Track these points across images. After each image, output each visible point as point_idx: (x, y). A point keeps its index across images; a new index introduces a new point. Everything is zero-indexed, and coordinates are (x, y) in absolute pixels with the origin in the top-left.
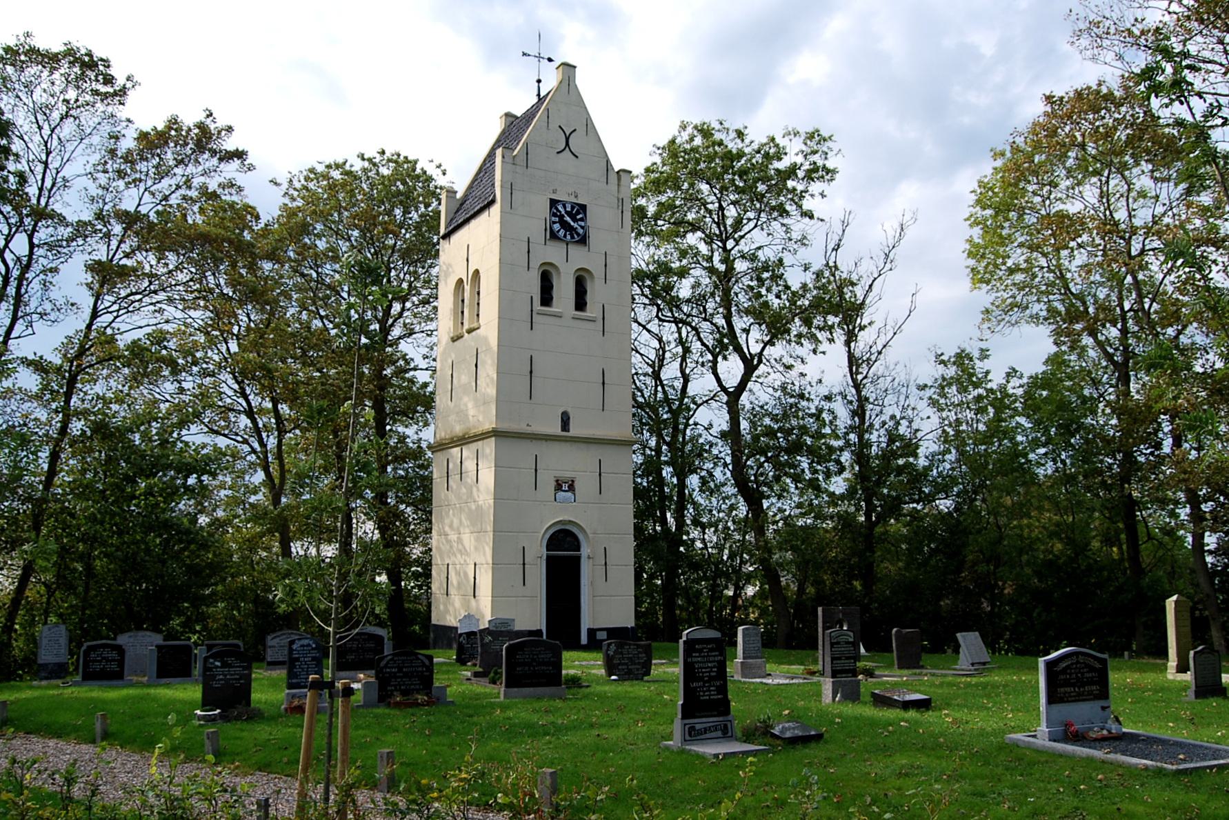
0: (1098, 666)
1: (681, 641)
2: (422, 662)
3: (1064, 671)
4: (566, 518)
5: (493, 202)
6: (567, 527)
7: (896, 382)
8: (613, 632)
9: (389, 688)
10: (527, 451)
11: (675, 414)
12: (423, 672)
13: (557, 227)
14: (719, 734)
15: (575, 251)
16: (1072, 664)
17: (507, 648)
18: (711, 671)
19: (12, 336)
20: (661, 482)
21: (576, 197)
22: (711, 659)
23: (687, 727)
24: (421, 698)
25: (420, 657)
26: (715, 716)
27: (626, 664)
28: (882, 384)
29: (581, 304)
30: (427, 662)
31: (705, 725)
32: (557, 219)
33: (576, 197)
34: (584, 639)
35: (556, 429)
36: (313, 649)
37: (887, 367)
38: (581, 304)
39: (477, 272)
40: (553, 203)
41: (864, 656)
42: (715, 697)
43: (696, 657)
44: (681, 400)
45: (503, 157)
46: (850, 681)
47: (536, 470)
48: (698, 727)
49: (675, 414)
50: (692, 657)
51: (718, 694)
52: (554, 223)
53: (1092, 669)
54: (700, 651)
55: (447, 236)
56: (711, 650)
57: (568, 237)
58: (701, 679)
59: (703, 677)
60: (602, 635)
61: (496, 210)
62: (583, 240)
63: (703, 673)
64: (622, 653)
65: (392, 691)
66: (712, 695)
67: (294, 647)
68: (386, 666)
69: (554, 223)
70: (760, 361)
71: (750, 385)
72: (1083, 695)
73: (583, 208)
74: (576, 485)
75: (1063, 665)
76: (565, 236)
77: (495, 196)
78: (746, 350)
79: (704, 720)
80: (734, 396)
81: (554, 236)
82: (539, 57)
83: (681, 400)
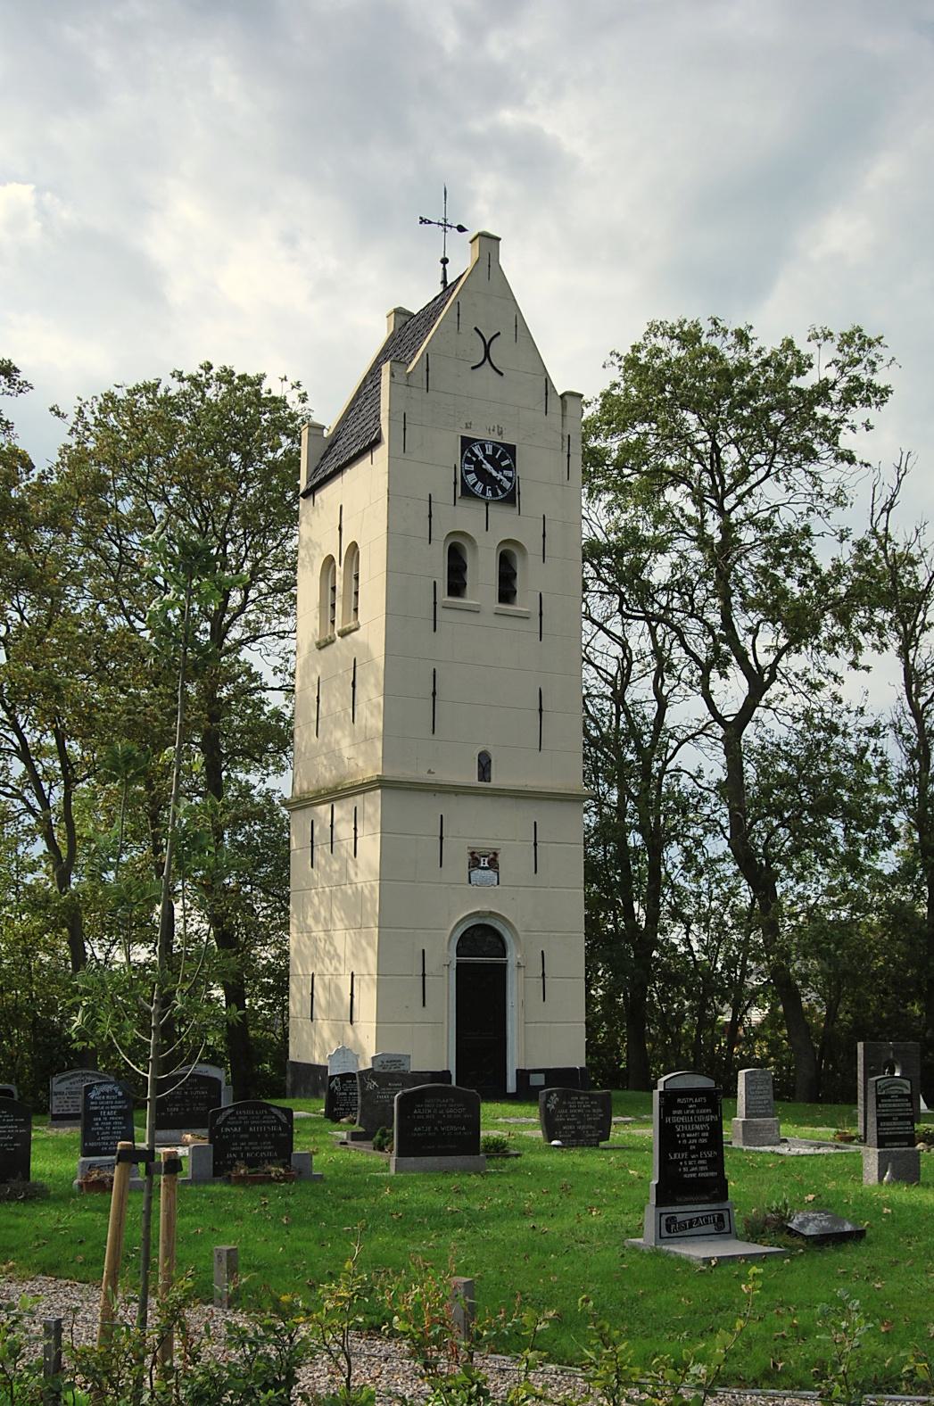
1: (656, 1093)
4: (486, 908)
5: (377, 442)
6: (487, 922)
8: (554, 1076)
10: (425, 811)
12: (277, 1132)
13: (471, 478)
14: (711, 1228)
15: (499, 513)
17: (400, 1099)
18: (100, 1122)
21: (500, 433)
22: (700, 1119)
23: (665, 1217)
24: (276, 1170)
25: (273, 1110)
27: (574, 1123)
29: (507, 593)
30: (284, 1119)
33: (500, 433)
34: (511, 1086)
35: (471, 778)
38: (507, 593)
39: (354, 546)
40: (467, 443)
42: (707, 1175)
43: (677, 1117)
45: (392, 375)
47: (441, 838)
48: (680, 1218)
49: (645, 755)
50: (672, 1115)
51: (709, 1171)
52: (468, 472)
54: (684, 1107)
55: (310, 492)
56: (700, 1106)
57: (489, 494)
58: (685, 1148)
60: (538, 1080)
61: (382, 453)
62: (511, 498)
63: (688, 1139)
64: (567, 1107)
65: (234, 1159)
66: (695, 1170)
67: (92, 1095)
68: (224, 1124)
73: (510, 450)
74: (499, 859)
76: (484, 492)
77: (380, 432)
81: (467, 492)
82: (445, 225)
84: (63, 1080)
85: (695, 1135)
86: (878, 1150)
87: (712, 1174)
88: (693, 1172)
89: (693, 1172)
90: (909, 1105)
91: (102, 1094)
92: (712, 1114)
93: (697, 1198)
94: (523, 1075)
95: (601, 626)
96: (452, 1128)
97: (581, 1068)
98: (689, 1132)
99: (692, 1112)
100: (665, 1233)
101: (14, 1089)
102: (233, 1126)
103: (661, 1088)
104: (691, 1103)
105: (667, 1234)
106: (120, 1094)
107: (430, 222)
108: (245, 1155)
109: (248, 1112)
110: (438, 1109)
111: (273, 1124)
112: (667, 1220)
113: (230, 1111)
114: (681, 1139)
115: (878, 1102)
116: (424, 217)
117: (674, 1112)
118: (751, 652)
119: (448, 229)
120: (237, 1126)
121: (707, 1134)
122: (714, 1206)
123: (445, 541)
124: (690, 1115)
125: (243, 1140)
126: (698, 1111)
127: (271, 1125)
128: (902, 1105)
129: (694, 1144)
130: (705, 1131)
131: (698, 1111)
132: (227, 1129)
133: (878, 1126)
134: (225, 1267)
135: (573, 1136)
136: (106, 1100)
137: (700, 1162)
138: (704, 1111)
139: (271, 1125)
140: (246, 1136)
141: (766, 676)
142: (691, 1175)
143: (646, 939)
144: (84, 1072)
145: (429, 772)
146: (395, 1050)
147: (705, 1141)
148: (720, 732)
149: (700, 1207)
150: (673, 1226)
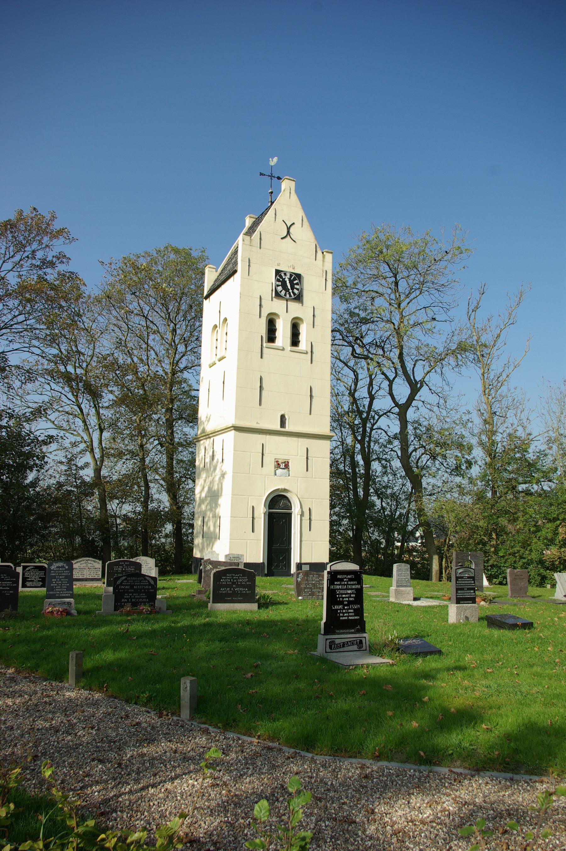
1: (325, 573)
2: (149, 581)
4: (280, 487)
5: (235, 272)
7: (515, 401)
9: (123, 600)
11: (364, 422)
13: (280, 288)
14: (355, 647)
15: (294, 306)
17: (214, 574)
18: (350, 597)
20: (354, 465)
21: (294, 268)
23: (328, 641)
24: (145, 608)
25: (147, 578)
27: (311, 588)
28: (504, 403)
29: (295, 341)
30: (152, 582)
32: (280, 283)
33: (294, 268)
34: (293, 569)
35: (277, 426)
36: (66, 570)
37: (509, 390)
38: (295, 341)
39: (226, 320)
40: (278, 272)
41: (487, 588)
43: (337, 586)
44: (368, 413)
45: (243, 241)
46: (470, 607)
47: (263, 454)
48: (337, 641)
49: (364, 422)
51: (355, 616)
52: (278, 286)
54: (342, 580)
55: (208, 297)
56: (350, 580)
57: (288, 296)
58: (341, 603)
59: (343, 601)
61: (237, 276)
62: (299, 298)
63: (343, 598)
64: (307, 580)
65: (125, 602)
66: (348, 614)
69: (278, 286)
70: (422, 386)
71: (414, 403)
73: (299, 276)
76: (285, 295)
79: (342, 636)
80: (403, 409)
81: (278, 295)
82: (271, 176)
83: (368, 413)
84: (77, 562)
85: (347, 596)
86: (456, 605)
87: (356, 617)
88: (346, 616)
89: (346, 616)
90: (472, 582)
91: (57, 567)
92: (357, 584)
93: (348, 631)
95: (346, 365)
96: (241, 589)
98: (344, 594)
102: (126, 585)
103: (328, 569)
104: (345, 578)
105: (330, 651)
106: (67, 567)
107: (264, 175)
108: (131, 600)
109: (134, 578)
110: (234, 579)
111: (147, 585)
112: (330, 643)
113: (124, 578)
115: (457, 580)
116: (262, 172)
117: (336, 583)
118: (411, 374)
119: (273, 178)
120: (128, 585)
121: (354, 596)
122: (357, 635)
123: (267, 317)
124: (344, 585)
125: (130, 593)
126: (349, 583)
127: (145, 585)
128: (469, 582)
129: (346, 601)
130: (353, 594)
131: (349, 583)
132: (123, 587)
133: (457, 593)
134: (75, 663)
135: (310, 595)
136: (59, 570)
137: (349, 611)
139: (145, 585)
140: (132, 591)
141: (419, 385)
143: (365, 504)
144: (87, 559)
145: (257, 423)
146: (236, 552)
148: (396, 410)
150: (333, 646)
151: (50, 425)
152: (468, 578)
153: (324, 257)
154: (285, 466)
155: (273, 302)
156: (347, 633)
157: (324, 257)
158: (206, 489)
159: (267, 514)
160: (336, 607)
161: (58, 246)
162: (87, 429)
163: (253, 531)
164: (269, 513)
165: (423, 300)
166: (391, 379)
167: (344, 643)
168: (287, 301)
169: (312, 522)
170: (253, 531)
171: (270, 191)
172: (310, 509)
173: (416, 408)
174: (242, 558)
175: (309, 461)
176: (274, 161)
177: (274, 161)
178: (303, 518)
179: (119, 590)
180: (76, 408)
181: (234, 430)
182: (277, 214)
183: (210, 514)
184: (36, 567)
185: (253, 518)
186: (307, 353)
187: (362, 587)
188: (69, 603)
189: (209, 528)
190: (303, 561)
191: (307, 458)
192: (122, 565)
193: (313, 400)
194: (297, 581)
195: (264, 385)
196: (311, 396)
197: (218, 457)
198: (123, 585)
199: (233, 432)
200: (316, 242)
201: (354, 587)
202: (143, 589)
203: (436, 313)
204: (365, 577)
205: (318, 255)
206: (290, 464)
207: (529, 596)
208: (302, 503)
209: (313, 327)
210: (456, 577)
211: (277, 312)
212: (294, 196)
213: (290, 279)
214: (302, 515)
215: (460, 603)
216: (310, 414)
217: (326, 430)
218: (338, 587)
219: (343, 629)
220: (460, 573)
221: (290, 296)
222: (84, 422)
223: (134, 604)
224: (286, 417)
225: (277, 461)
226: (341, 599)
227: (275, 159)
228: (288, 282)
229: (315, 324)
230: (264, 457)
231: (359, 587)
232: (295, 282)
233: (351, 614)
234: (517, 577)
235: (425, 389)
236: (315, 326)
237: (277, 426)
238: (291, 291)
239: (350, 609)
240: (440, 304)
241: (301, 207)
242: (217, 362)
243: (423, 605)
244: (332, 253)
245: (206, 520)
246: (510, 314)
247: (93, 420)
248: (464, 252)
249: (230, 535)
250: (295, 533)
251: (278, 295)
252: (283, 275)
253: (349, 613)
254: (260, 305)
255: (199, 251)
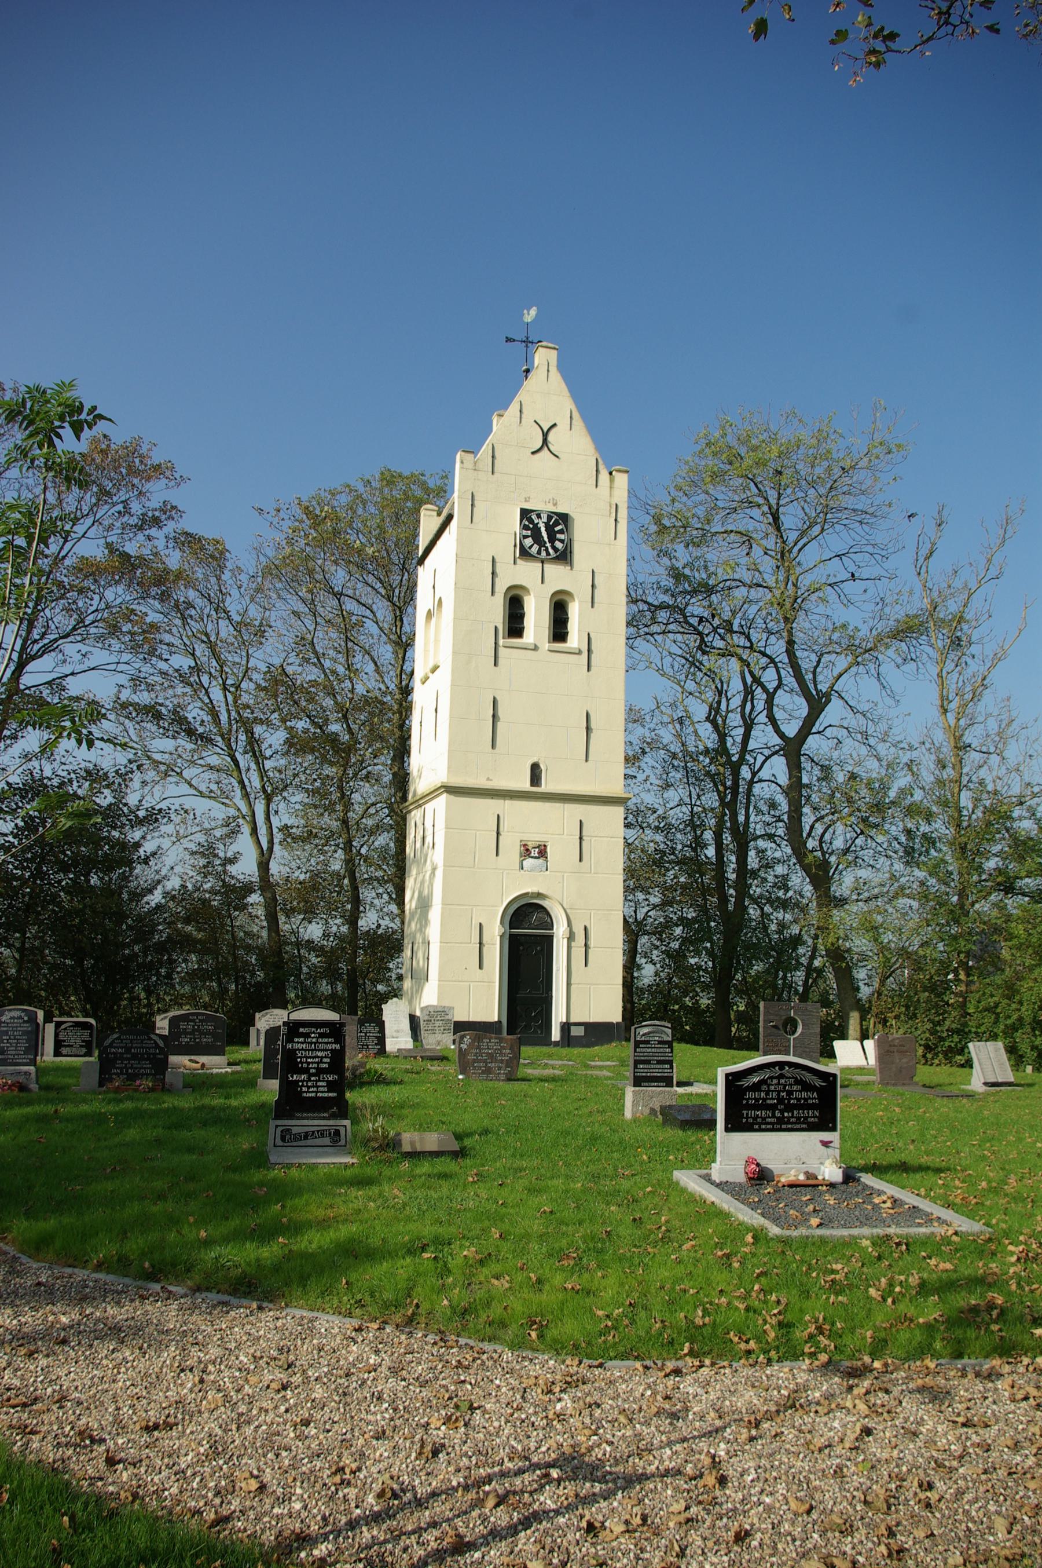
0: (818, 1083)
3: (756, 1087)
4: (529, 890)
12: (155, 1054)
13: (528, 542)
14: (327, 1141)
15: (554, 571)
16: (771, 1078)
18: (322, 1062)
19: (814, 730)
21: (555, 505)
22: (321, 1047)
23: (280, 1129)
26: (324, 1118)
27: (485, 1061)
29: (559, 631)
31: (306, 1129)
32: (529, 533)
33: (555, 505)
34: (556, 1035)
35: (525, 785)
36: (25, 1022)
38: (559, 631)
39: (440, 599)
40: (525, 513)
42: (326, 1095)
45: (462, 462)
47: (498, 833)
48: (295, 1130)
51: (328, 1092)
52: (525, 537)
53: (806, 1087)
54: (307, 1035)
56: (322, 1035)
57: (544, 553)
60: (577, 1032)
61: (454, 523)
62: (564, 557)
63: (308, 1064)
64: (479, 1047)
68: (111, 1045)
69: (525, 537)
70: (828, 701)
72: (788, 1123)
73: (564, 518)
75: (755, 1079)
76: (539, 553)
78: (811, 686)
79: (311, 1122)
81: (525, 553)
86: (633, 1089)
87: (331, 1095)
91: (11, 1018)
92: (335, 1042)
93: (316, 1115)
94: (566, 1027)
97: (618, 1023)
98: (310, 1057)
99: (314, 1040)
100: (279, 1142)
101: (92, 1021)
105: (281, 1144)
106: (26, 1018)
109: (132, 1037)
114: (302, 1063)
116: (510, 336)
117: (296, 1040)
122: (331, 1122)
123: (506, 593)
124: (311, 1043)
126: (320, 1040)
127: (149, 1048)
130: (326, 1057)
132: (113, 1050)
133: (635, 1067)
135: (483, 1072)
137: (319, 1084)
138: (326, 1040)
139: (149, 1048)
142: (310, 1095)
145: (488, 779)
147: (326, 1066)
149: (316, 1122)
151: (185, 789)
152: (660, 1042)
153: (612, 481)
154: (540, 852)
155: (517, 566)
156: (314, 1118)
157: (612, 481)
158: (416, 895)
159: (508, 936)
160: (295, 1076)
161: (158, 493)
162: (246, 795)
163: (481, 967)
164: (511, 935)
165: (836, 540)
166: (771, 690)
167: (306, 1133)
168: (543, 562)
169: (590, 951)
170: (481, 967)
171: (525, 368)
172: (586, 928)
173: (835, 741)
174: (451, 1014)
175: (584, 843)
176: (530, 315)
177: (530, 315)
178: (573, 944)
179: (107, 1054)
180: (229, 759)
181: (447, 792)
182: (524, 410)
183: (419, 939)
184: (77, 1024)
185: (480, 943)
186: (580, 652)
187: (343, 1048)
188: (27, 1074)
189: (418, 962)
190: (572, 1020)
191: (581, 838)
192: (192, 1021)
193: (593, 736)
194: (460, 1049)
195: (501, 713)
196: (588, 729)
197: (429, 840)
198: (115, 1047)
199: (444, 797)
200: (597, 455)
201: (329, 1047)
202: (146, 1053)
203: (861, 565)
204: (675, 1044)
205: (601, 477)
206: (548, 850)
207: (916, 1084)
208: (571, 917)
209: (592, 607)
210: (635, 1041)
211: (524, 584)
212: (555, 375)
213: (547, 525)
214: (571, 938)
215: (640, 1086)
216: (587, 760)
217: (616, 787)
218: (300, 1046)
219: (308, 1111)
220: (644, 1035)
221: (548, 554)
222: (241, 782)
223: (132, 1077)
224: (542, 767)
225: (525, 845)
226: (305, 1065)
227: (533, 312)
228: (543, 529)
229: (596, 600)
230: (501, 838)
231: (338, 1047)
232: (557, 529)
233: (321, 1089)
234: (892, 1049)
235: (835, 705)
236: (596, 605)
237: (525, 785)
238: (548, 545)
239: (319, 1080)
240: (870, 549)
241: (568, 394)
242: (430, 675)
243: (700, 1091)
244: (627, 472)
245: (415, 948)
246: (989, 561)
247: (254, 781)
248: (894, 450)
249: (440, 973)
250: (558, 970)
251: (525, 553)
252: (534, 517)
253: (318, 1087)
254: (493, 573)
255: (437, 477)
